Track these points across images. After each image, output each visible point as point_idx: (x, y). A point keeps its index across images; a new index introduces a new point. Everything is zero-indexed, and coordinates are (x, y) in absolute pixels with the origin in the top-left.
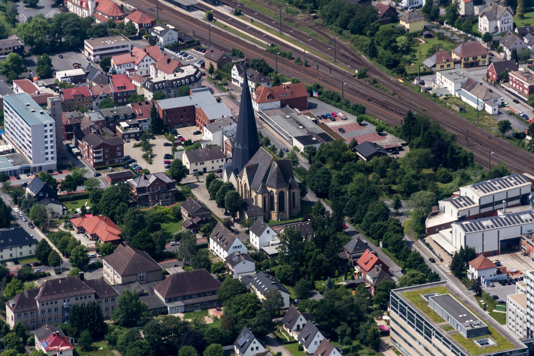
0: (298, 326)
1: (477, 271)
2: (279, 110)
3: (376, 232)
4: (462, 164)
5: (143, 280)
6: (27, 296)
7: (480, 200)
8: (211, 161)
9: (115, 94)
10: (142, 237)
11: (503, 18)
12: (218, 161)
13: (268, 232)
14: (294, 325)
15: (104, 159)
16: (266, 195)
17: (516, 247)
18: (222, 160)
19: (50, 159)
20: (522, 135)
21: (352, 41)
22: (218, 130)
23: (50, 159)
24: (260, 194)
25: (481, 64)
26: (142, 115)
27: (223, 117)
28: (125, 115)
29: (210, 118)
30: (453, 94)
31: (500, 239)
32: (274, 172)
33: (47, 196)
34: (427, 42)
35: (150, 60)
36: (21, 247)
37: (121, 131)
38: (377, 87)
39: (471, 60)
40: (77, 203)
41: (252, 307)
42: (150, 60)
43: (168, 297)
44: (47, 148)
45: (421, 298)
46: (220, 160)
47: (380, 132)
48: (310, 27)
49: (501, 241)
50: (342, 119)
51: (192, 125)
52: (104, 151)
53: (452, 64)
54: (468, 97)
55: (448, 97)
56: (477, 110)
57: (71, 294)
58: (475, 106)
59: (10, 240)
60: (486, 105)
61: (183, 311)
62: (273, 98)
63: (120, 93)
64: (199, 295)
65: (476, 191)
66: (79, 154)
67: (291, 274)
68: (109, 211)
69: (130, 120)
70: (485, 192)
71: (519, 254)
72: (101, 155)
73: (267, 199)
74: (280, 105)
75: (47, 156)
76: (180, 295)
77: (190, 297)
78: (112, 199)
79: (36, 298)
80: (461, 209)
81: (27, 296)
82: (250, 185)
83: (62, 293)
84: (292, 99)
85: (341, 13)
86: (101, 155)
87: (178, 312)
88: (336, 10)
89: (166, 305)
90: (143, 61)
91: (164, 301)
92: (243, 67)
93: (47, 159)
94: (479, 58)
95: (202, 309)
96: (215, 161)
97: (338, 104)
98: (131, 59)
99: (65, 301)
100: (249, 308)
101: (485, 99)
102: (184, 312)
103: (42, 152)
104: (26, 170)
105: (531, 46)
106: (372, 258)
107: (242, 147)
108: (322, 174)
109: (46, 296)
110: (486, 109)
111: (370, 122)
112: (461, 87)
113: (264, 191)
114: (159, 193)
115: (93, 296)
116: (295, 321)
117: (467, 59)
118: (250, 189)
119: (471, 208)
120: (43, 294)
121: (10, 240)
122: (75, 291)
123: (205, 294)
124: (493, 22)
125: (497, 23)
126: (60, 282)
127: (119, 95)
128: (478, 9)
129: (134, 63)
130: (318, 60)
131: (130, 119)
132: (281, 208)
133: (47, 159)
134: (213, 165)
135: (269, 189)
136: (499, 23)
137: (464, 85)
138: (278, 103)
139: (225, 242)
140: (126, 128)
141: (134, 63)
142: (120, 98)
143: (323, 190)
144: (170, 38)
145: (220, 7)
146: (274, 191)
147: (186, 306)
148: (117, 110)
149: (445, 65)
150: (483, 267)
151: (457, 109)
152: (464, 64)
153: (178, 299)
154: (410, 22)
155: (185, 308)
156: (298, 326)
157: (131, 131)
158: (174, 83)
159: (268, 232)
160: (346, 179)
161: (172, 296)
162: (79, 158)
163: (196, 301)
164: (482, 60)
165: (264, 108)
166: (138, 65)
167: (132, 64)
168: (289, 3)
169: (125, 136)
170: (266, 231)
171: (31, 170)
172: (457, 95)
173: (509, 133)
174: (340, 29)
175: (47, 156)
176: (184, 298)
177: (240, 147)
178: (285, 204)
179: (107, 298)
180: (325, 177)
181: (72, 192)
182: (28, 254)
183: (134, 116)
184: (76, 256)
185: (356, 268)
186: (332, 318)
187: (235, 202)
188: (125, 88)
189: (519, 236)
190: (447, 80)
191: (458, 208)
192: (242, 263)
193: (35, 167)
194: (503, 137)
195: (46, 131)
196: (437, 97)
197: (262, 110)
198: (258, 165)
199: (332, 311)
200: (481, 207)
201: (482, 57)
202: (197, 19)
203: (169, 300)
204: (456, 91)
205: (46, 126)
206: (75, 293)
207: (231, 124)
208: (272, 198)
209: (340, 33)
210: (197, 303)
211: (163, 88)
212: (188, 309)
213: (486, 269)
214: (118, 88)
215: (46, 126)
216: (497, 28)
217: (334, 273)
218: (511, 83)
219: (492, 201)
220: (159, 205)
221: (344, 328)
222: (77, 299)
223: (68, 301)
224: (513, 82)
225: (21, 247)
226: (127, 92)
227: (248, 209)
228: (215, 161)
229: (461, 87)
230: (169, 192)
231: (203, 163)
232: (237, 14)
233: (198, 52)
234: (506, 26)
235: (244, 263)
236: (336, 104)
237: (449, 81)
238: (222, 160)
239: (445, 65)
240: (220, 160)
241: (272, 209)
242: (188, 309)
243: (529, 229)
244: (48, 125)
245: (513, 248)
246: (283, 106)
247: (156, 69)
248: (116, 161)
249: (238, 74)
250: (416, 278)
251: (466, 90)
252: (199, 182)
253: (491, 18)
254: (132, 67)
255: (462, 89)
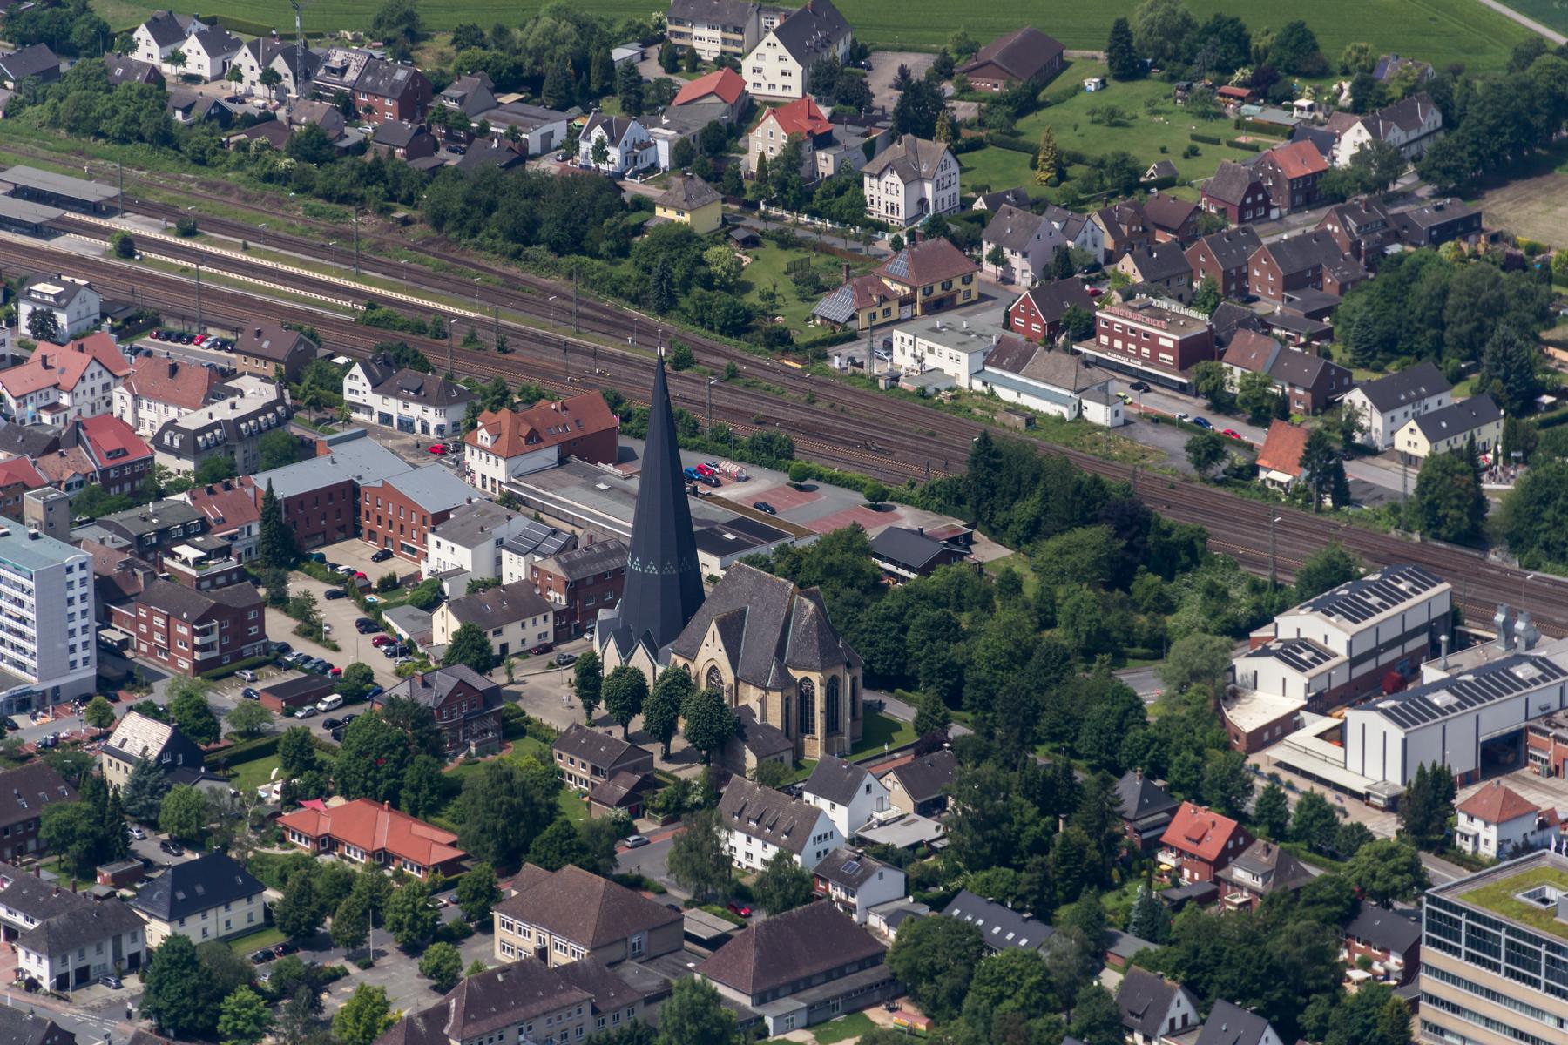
0: (1172, 1021)
1: (1494, 829)
2: (560, 473)
3: (1142, 758)
4: (1185, 559)
5: (641, 954)
6: (424, 1030)
7: (1350, 644)
8: (519, 624)
9: (104, 473)
10: (564, 838)
11: (938, 176)
12: (534, 622)
13: (868, 788)
14: (1163, 1019)
15: (223, 649)
16: (792, 692)
17: (1510, 758)
18: (545, 618)
19: (80, 664)
20: (1246, 472)
21: (570, 276)
22: (485, 540)
23: (80, 664)
24: (774, 689)
25: (960, 300)
26: (224, 521)
27: (470, 501)
28: (184, 526)
29: (433, 509)
30: (963, 382)
31: (1481, 740)
32: (808, 626)
33: (180, 763)
34: (757, 258)
35: (100, 374)
36: (227, 908)
37: (193, 572)
38: (747, 386)
39: (938, 291)
40: (236, 775)
41: (1037, 986)
42: (100, 374)
43: (758, 989)
44: (72, 633)
45: (1520, 903)
46: (540, 618)
47: (879, 501)
48: (411, 249)
49: (1484, 743)
50: (739, 480)
51: (347, 538)
52: (221, 625)
53: (894, 306)
54: (1020, 389)
55: (957, 394)
56: (1061, 420)
57: (535, 1009)
58: (1052, 409)
59: (200, 889)
60: (1085, 403)
61: (804, 1022)
62: (540, 440)
63: (114, 468)
64: (829, 976)
65: (1333, 619)
66: (124, 644)
67: (1031, 892)
68: (377, 782)
69: (198, 539)
70: (1357, 622)
71: (1526, 772)
72: (214, 637)
73: (793, 704)
74: (556, 458)
75: (72, 657)
76: (785, 979)
77: (808, 983)
78: (386, 749)
79: (446, 1031)
80: (1311, 672)
81: (424, 1030)
82: (734, 667)
83: (510, 1009)
84: (581, 438)
85: (501, 201)
86: (214, 637)
87: (793, 1029)
88: (484, 194)
89: (759, 1011)
90: (83, 378)
91: (746, 1001)
92: (379, 366)
93: (73, 664)
94: (957, 284)
95: (848, 1013)
96: (529, 622)
97: (697, 440)
98: (47, 378)
99: (521, 1032)
100: (1032, 988)
101: (1079, 387)
102: (807, 1027)
103: (60, 646)
104: (23, 701)
105: (1073, 240)
106: (1214, 824)
107: (661, 567)
108: (883, 620)
109: (474, 1021)
110: (1085, 413)
111: (820, 478)
112: (985, 363)
113: (784, 683)
114: (466, 722)
115: (587, 1008)
116: (1166, 1009)
117: (928, 291)
118: (737, 680)
119: (1333, 668)
120: (466, 1019)
121: (200, 889)
122: (562, 991)
123: (841, 972)
124: (915, 187)
125: (922, 189)
126: (500, 978)
127: (112, 474)
128: (831, 158)
129: (56, 386)
130: (521, 331)
131: (197, 534)
132: (832, 726)
133: (73, 664)
134: (522, 634)
135: (798, 675)
136: (929, 189)
137: (991, 356)
138: (552, 454)
139: (783, 826)
140: (198, 562)
141: (56, 386)
142: (114, 482)
143: (890, 666)
144: (84, 314)
145: (116, 219)
146: (816, 677)
147: (811, 1008)
148: (155, 515)
149: (879, 312)
150: (1507, 815)
151: (1018, 420)
152: (923, 304)
153: (781, 993)
154: (691, 210)
155: (809, 1014)
156: (1172, 1021)
157: (216, 566)
158: (243, 426)
159: (868, 788)
160: (948, 629)
161: (767, 985)
162: (129, 654)
163: (833, 992)
164: (964, 288)
165: (521, 470)
166: (70, 391)
167: (51, 391)
168: (297, 191)
169: (205, 584)
170: (863, 788)
171: (35, 702)
172: (978, 385)
173: (1219, 469)
174: (513, 247)
175: (72, 657)
176: (794, 989)
177: (653, 569)
178: (841, 714)
179: (618, 1009)
180: (890, 629)
181: (213, 745)
182: (245, 925)
183: (205, 527)
184: (413, 910)
185: (1161, 857)
186: (1270, 988)
187: (720, 720)
188: (126, 453)
189: (1523, 724)
190: (937, 347)
191: (1303, 670)
192: (876, 876)
193: (44, 692)
194: (1203, 480)
195: (70, 585)
196: (929, 397)
197: (517, 477)
198: (743, 612)
199: (1270, 968)
200: (1354, 662)
201: (964, 282)
202: (81, 258)
203: (761, 999)
204: (972, 376)
205: (70, 570)
206: (545, 1005)
207: (509, 518)
208: (806, 700)
209: (517, 256)
210: (836, 998)
211: (217, 444)
212: (817, 1017)
213: (1516, 817)
214: (109, 454)
215: (70, 570)
216: (923, 202)
217: (1111, 880)
218: (1104, 339)
219: (1372, 645)
220: (469, 755)
221: (1320, 1011)
222: (550, 1021)
223: (530, 1028)
224: (1113, 336)
225: (227, 908)
226: (132, 464)
227: (750, 737)
228: (529, 622)
229: (985, 363)
230: (486, 716)
231: (500, 631)
232: (188, 233)
233: (179, 345)
234: (945, 194)
235: (881, 875)
236: (691, 440)
237: (946, 351)
238: (545, 618)
239: (879, 312)
240: (540, 618)
241: (806, 726)
242: (817, 1017)
243: (1543, 703)
244: (76, 568)
245: (1502, 759)
246: (562, 461)
247: (135, 398)
248: (247, 650)
249: (369, 386)
250: (1402, 860)
251: (1003, 368)
252: (512, 683)
253: (909, 177)
254: (51, 401)
255: (987, 368)
